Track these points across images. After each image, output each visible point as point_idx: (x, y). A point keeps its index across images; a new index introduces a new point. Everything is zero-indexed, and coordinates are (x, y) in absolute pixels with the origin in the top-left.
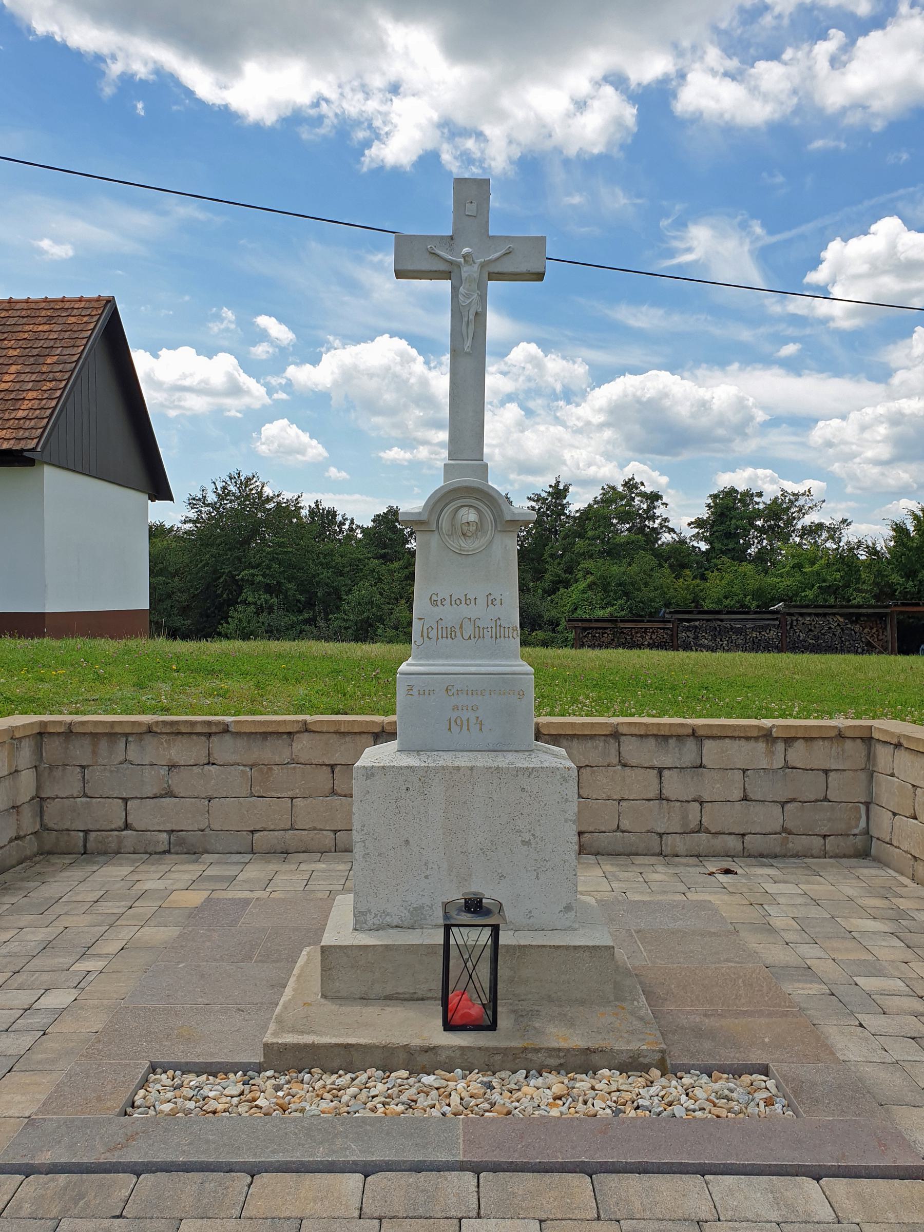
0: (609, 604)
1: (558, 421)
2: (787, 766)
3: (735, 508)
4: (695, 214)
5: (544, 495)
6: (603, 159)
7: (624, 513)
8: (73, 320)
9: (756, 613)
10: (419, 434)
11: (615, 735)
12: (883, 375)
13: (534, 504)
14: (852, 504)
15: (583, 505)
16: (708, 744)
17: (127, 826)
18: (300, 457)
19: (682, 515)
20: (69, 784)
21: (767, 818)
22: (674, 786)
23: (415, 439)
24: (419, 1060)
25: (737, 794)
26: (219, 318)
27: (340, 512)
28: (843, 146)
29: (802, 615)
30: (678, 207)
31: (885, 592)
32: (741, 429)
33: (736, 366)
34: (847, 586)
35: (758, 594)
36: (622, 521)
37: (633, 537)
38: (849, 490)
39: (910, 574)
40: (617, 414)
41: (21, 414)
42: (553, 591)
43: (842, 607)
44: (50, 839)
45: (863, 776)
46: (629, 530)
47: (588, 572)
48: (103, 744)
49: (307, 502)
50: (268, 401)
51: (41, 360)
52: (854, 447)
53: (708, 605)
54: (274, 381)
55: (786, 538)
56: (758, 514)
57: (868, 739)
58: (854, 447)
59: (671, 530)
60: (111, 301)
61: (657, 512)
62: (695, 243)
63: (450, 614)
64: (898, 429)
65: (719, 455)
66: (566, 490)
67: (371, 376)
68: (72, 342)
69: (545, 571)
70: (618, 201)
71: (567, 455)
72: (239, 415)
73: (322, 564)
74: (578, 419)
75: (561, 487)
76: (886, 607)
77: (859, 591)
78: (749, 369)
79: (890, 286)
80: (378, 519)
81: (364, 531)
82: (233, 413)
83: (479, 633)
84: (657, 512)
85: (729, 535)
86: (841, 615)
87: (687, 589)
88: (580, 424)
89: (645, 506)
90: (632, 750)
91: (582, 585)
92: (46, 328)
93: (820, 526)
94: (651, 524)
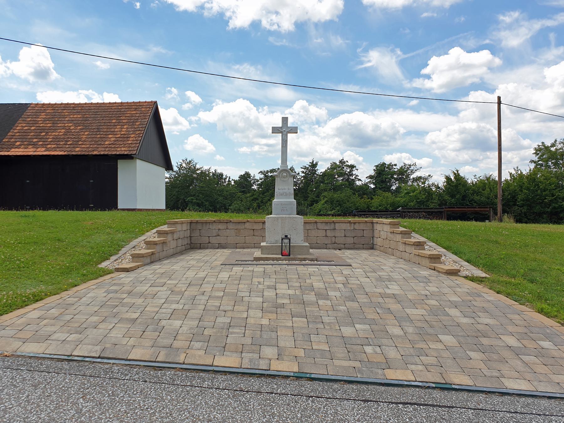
0: (334, 209)
1: (315, 134)
2: (354, 229)
3: (384, 170)
4: (373, 45)
5: (307, 166)
6: (331, 22)
7: (341, 172)
8: (143, 109)
9: (391, 211)
10: (255, 140)
11: (316, 222)
12: (455, 113)
13: (303, 170)
14: (443, 168)
15: (323, 170)
16: (336, 224)
17: (209, 243)
18: (204, 151)
19: (364, 173)
20: (197, 233)
21: (350, 240)
22: (329, 233)
23: (253, 143)
24: (277, 259)
25: (343, 235)
26: (170, 92)
27: (225, 174)
28: (435, 15)
29: (409, 212)
30: (364, 44)
31: (443, 203)
32: (393, 137)
33: (391, 110)
34: (427, 201)
35: (393, 204)
36: (339, 176)
37: (344, 183)
38: (442, 162)
39: (453, 196)
40: (340, 132)
41: (130, 142)
42: (312, 205)
43: (424, 209)
44: (192, 245)
45: (371, 231)
46: (342, 180)
47: (325, 197)
48: (204, 225)
49: (212, 170)
50: (189, 127)
51: (134, 124)
52: (444, 144)
53: (373, 209)
54: (193, 118)
55: (406, 182)
56: (395, 173)
57: (372, 223)
58: (444, 144)
59: (359, 180)
60: (156, 102)
61: (354, 173)
62: (372, 59)
63: (281, 191)
64: (463, 136)
65: (385, 148)
66: (317, 164)
67: (234, 116)
68: (144, 117)
69: (308, 197)
70: (338, 42)
71: (318, 148)
72: (178, 133)
73: (219, 195)
74: (324, 133)
75: (314, 163)
76: (443, 209)
77: (433, 203)
78: (397, 111)
79: (458, 74)
80: (241, 177)
81: (235, 182)
82: (175, 133)
83: (286, 195)
84: (354, 173)
85: (382, 182)
86: (425, 212)
87: (365, 203)
88: (325, 135)
89: (349, 170)
90: (319, 226)
91: (323, 202)
92: (135, 112)
93: (420, 178)
94: (351, 177)
